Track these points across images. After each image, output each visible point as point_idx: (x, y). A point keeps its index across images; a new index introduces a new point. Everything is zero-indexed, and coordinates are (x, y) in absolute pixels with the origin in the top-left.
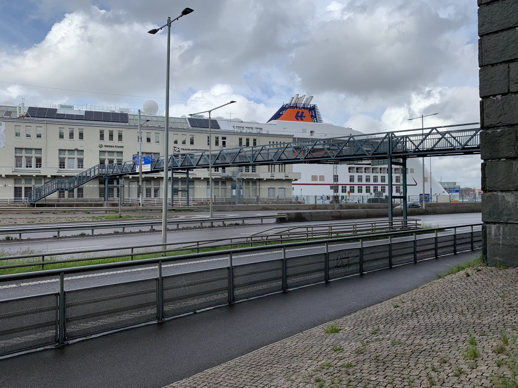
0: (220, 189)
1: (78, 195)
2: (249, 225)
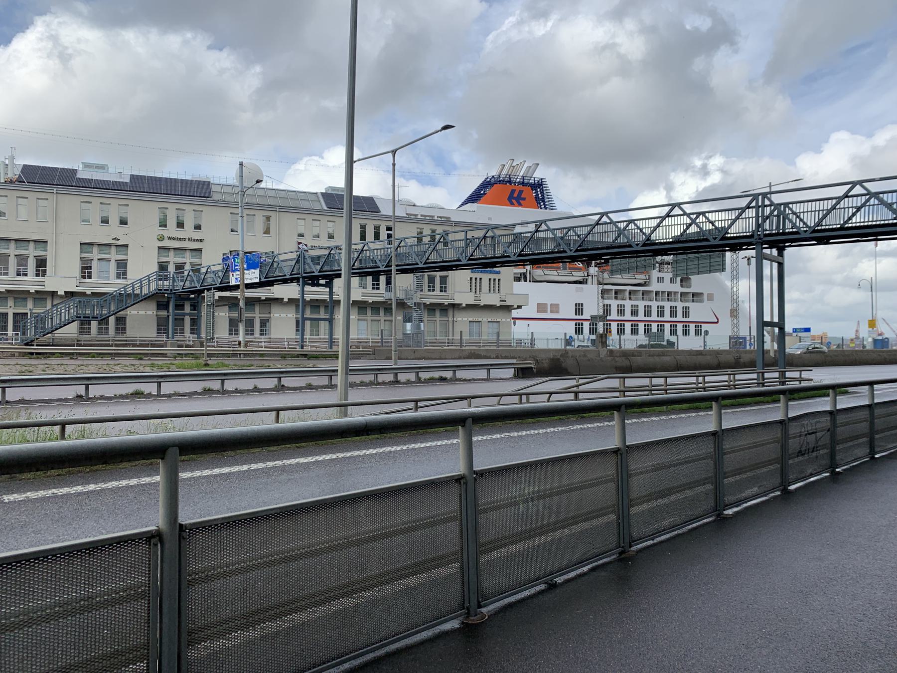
0: (382, 321)
1: (117, 329)
2: (465, 380)
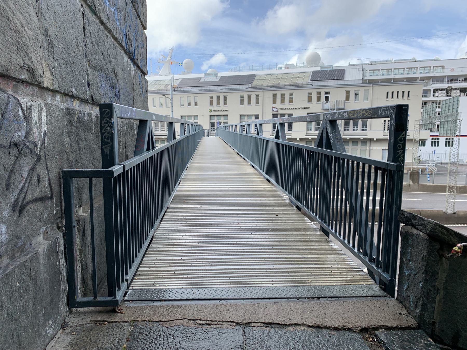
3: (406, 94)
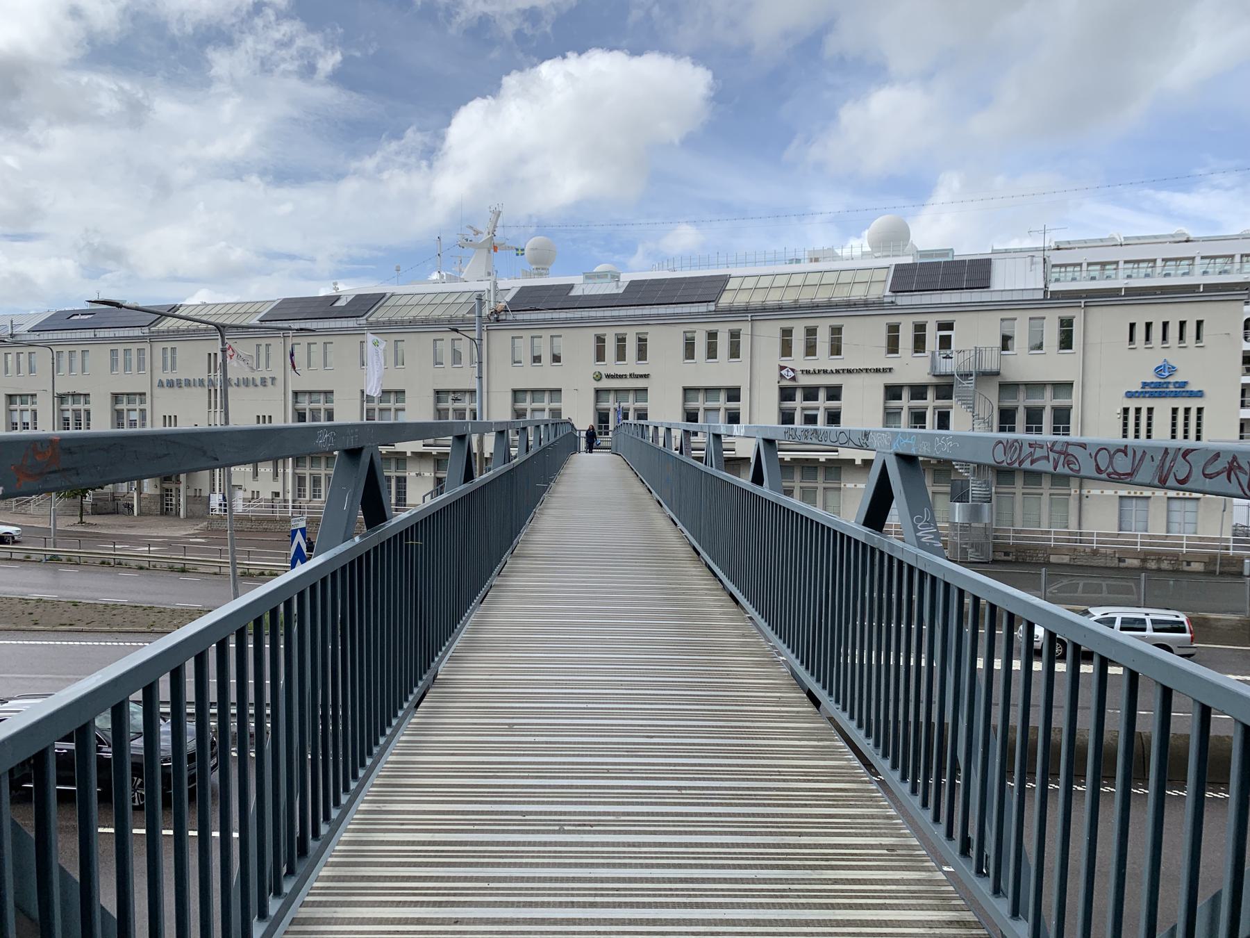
0: (1019, 497)
3: (1190, 330)
